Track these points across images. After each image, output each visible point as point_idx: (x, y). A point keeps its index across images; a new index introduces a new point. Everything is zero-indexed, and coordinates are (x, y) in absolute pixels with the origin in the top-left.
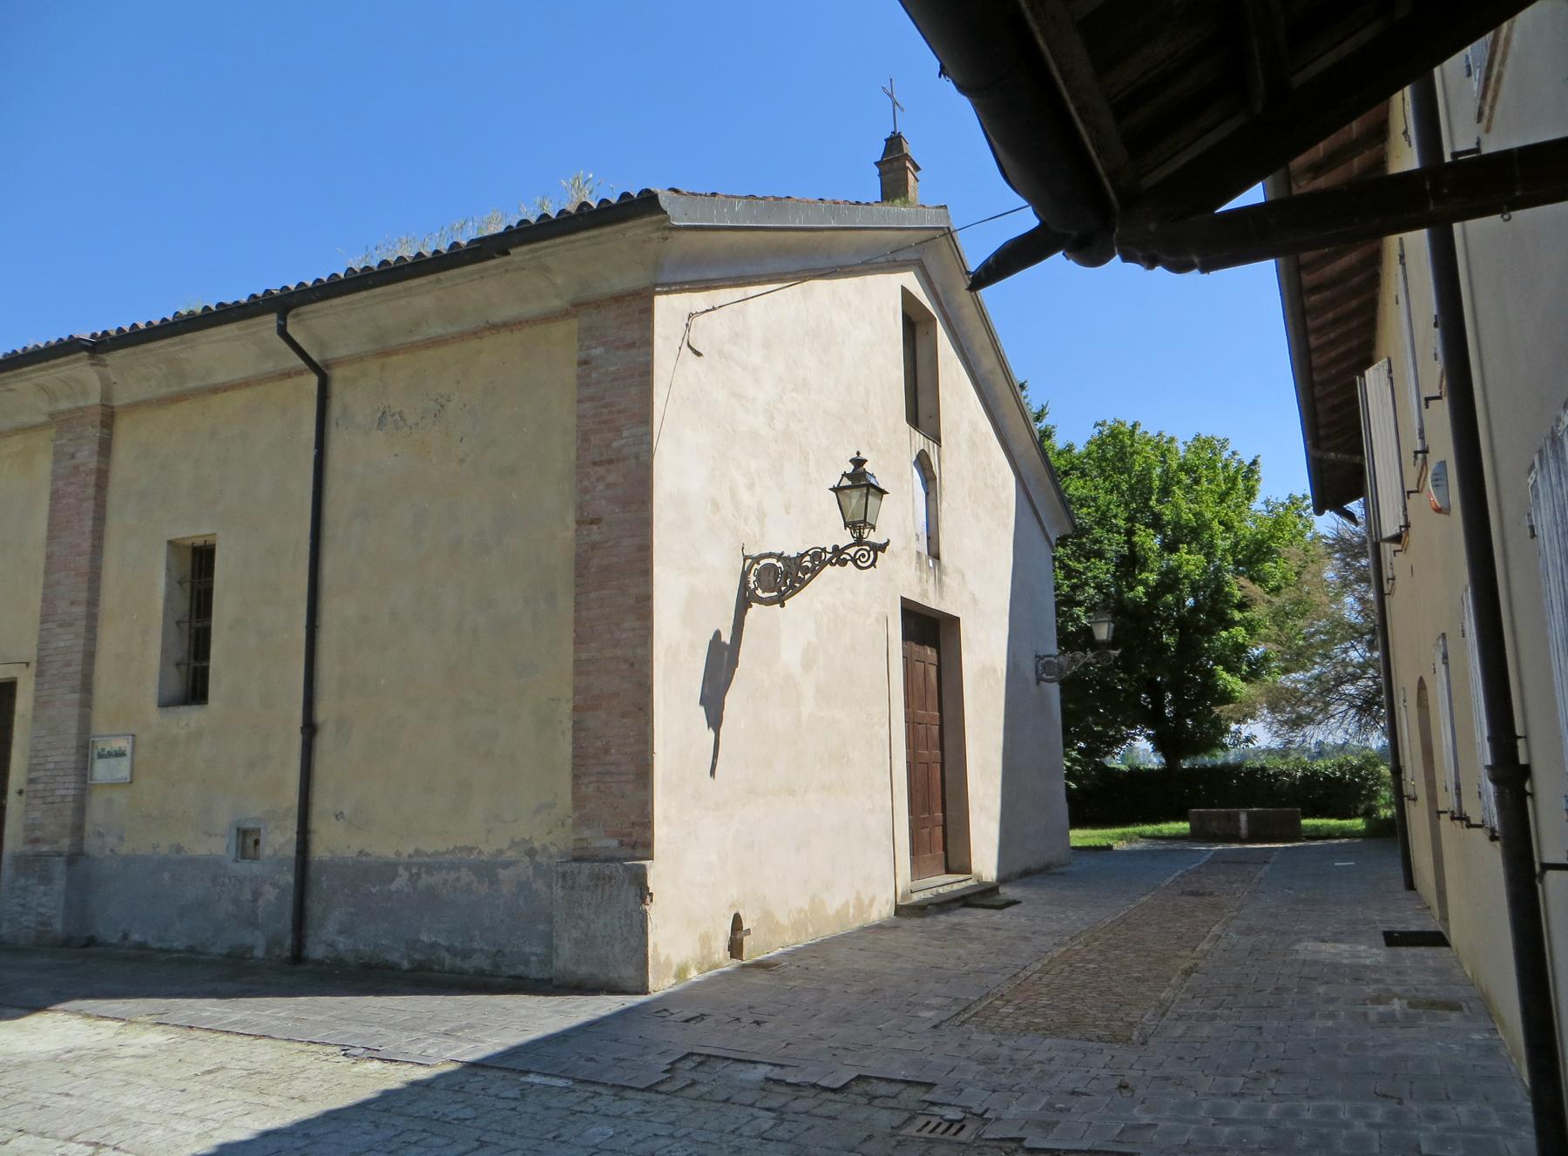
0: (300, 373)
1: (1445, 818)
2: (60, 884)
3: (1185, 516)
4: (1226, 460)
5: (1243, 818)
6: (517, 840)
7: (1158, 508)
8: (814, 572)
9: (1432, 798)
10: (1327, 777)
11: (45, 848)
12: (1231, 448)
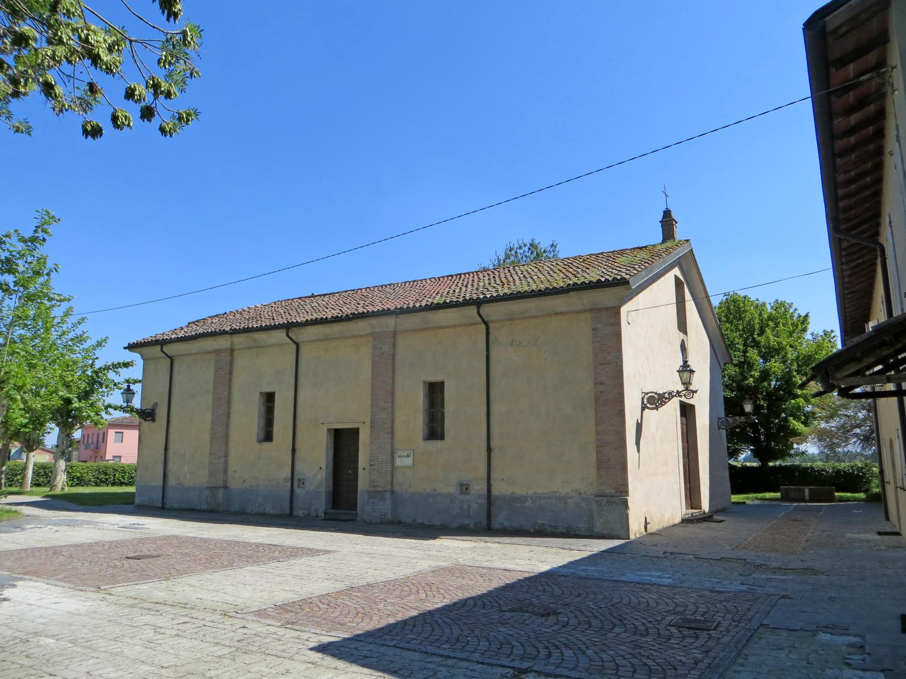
0: (480, 324)
1: (899, 489)
2: (389, 502)
3: (772, 343)
4: (792, 313)
5: (807, 491)
6: (574, 489)
7: (759, 339)
8: (669, 399)
9: (895, 482)
10: (845, 472)
11: (380, 489)
12: (794, 307)
